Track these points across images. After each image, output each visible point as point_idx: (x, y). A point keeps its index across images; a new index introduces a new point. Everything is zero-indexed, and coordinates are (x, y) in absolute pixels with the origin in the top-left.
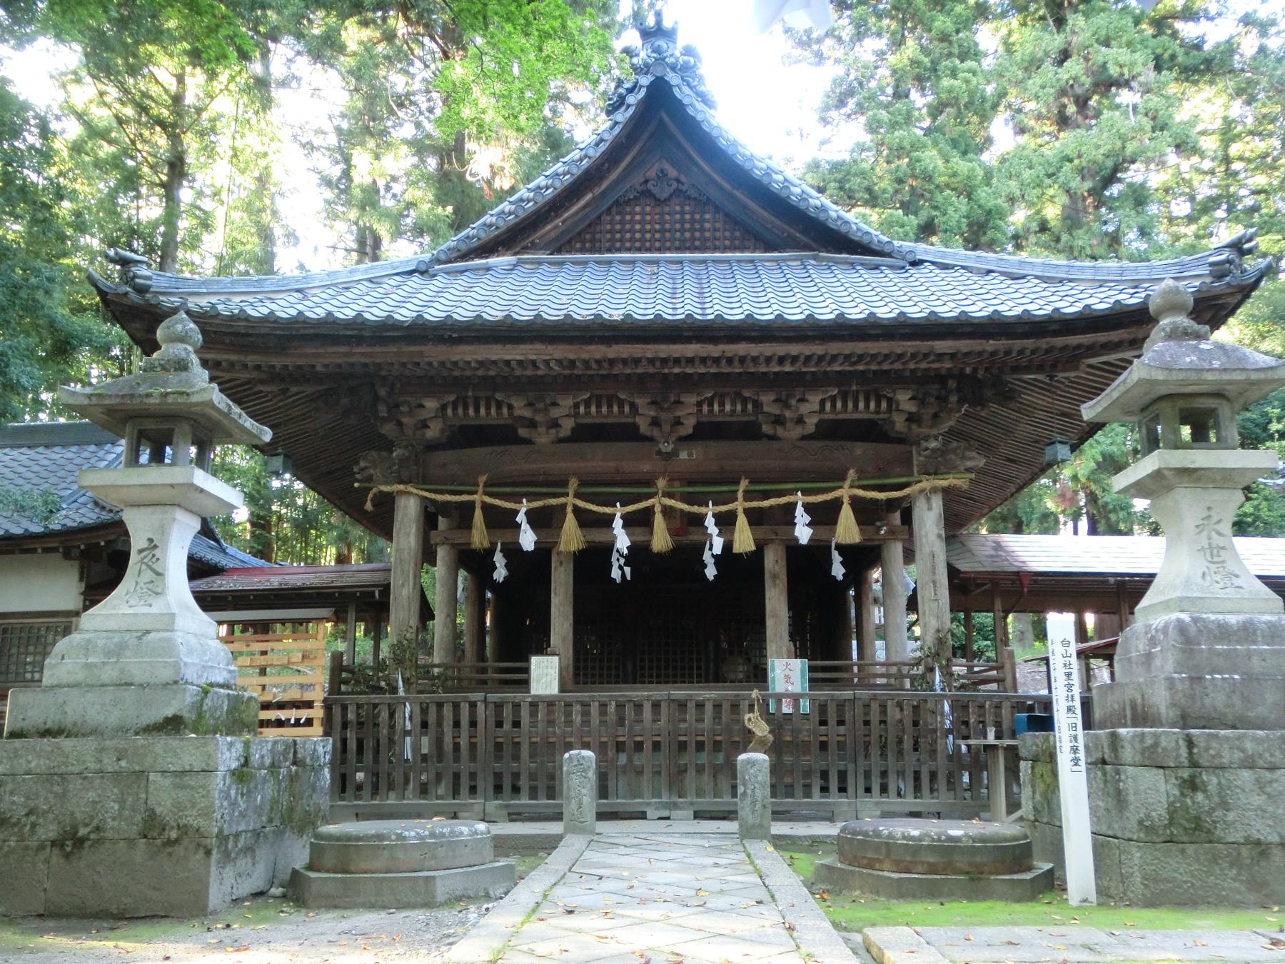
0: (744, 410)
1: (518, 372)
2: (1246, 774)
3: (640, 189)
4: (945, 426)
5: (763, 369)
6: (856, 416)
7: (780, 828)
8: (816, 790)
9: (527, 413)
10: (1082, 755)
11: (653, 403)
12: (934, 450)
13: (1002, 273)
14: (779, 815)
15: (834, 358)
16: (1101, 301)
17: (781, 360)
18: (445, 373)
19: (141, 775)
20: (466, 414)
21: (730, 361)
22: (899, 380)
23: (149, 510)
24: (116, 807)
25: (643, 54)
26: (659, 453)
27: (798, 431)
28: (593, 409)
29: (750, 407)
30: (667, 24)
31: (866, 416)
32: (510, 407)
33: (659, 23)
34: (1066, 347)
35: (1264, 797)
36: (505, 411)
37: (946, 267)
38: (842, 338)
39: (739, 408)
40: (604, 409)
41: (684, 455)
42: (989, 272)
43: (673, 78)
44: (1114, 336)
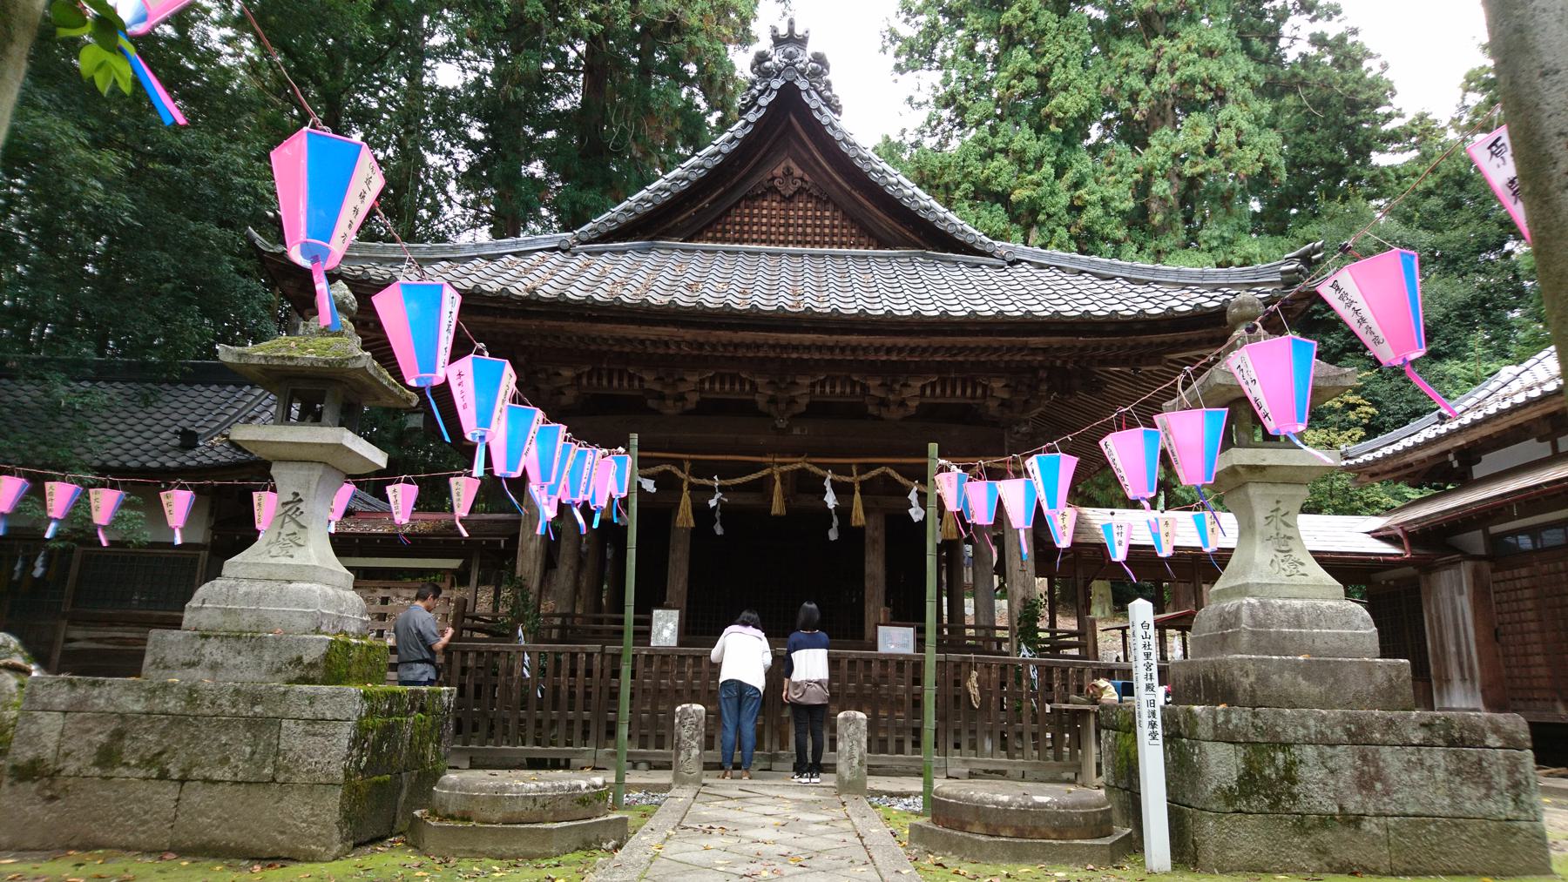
0: (853, 392)
1: (651, 350)
2: (1309, 750)
3: (766, 184)
4: (1035, 413)
5: (872, 357)
6: (953, 401)
7: (875, 783)
8: (908, 746)
9: (657, 387)
10: (1159, 729)
11: (771, 383)
12: (1024, 434)
13: (1093, 274)
14: (874, 771)
15: (936, 350)
16: (1182, 302)
17: (889, 351)
18: (582, 346)
19: (276, 722)
20: (599, 383)
21: (843, 349)
22: (995, 370)
23: (297, 465)
24: (248, 750)
25: (776, 59)
26: (775, 428)
27: (901, 412)
28: (717, 386)
29: (858, 389)
30: (799, 31)
31: (963, 401)
32: (641, 380)
33: (791, 30)
34: (1151, 344)
35: (1325, 771)
36: (636, 383)
37: (1041, 266)
38: (945, 333)
39: (848, 390)
40: (727, 387)
41: (796, 431)
42: (1081, 272)
43: (802, 84)
44: (1194, 335)
